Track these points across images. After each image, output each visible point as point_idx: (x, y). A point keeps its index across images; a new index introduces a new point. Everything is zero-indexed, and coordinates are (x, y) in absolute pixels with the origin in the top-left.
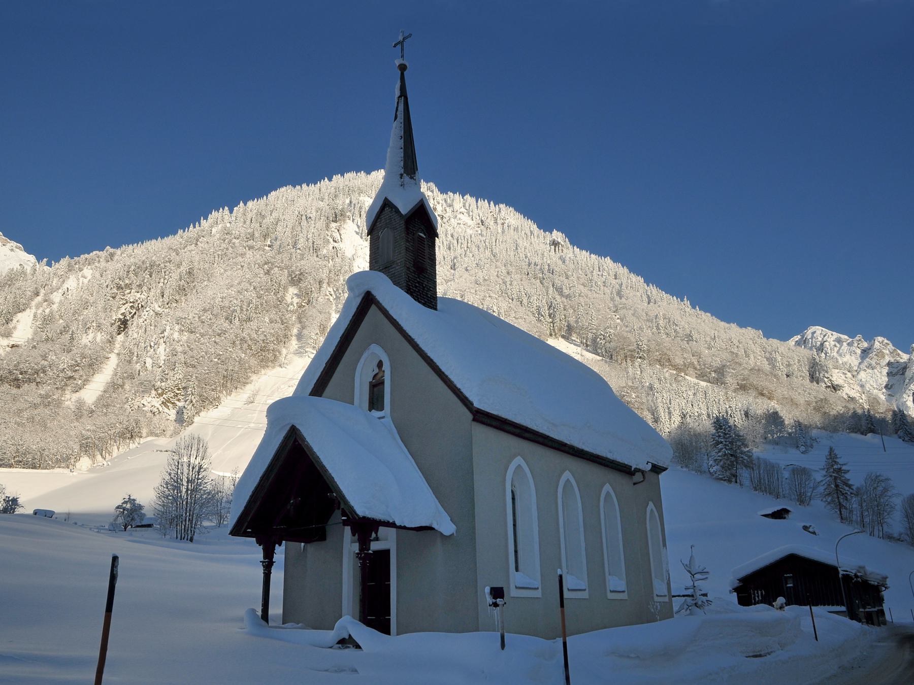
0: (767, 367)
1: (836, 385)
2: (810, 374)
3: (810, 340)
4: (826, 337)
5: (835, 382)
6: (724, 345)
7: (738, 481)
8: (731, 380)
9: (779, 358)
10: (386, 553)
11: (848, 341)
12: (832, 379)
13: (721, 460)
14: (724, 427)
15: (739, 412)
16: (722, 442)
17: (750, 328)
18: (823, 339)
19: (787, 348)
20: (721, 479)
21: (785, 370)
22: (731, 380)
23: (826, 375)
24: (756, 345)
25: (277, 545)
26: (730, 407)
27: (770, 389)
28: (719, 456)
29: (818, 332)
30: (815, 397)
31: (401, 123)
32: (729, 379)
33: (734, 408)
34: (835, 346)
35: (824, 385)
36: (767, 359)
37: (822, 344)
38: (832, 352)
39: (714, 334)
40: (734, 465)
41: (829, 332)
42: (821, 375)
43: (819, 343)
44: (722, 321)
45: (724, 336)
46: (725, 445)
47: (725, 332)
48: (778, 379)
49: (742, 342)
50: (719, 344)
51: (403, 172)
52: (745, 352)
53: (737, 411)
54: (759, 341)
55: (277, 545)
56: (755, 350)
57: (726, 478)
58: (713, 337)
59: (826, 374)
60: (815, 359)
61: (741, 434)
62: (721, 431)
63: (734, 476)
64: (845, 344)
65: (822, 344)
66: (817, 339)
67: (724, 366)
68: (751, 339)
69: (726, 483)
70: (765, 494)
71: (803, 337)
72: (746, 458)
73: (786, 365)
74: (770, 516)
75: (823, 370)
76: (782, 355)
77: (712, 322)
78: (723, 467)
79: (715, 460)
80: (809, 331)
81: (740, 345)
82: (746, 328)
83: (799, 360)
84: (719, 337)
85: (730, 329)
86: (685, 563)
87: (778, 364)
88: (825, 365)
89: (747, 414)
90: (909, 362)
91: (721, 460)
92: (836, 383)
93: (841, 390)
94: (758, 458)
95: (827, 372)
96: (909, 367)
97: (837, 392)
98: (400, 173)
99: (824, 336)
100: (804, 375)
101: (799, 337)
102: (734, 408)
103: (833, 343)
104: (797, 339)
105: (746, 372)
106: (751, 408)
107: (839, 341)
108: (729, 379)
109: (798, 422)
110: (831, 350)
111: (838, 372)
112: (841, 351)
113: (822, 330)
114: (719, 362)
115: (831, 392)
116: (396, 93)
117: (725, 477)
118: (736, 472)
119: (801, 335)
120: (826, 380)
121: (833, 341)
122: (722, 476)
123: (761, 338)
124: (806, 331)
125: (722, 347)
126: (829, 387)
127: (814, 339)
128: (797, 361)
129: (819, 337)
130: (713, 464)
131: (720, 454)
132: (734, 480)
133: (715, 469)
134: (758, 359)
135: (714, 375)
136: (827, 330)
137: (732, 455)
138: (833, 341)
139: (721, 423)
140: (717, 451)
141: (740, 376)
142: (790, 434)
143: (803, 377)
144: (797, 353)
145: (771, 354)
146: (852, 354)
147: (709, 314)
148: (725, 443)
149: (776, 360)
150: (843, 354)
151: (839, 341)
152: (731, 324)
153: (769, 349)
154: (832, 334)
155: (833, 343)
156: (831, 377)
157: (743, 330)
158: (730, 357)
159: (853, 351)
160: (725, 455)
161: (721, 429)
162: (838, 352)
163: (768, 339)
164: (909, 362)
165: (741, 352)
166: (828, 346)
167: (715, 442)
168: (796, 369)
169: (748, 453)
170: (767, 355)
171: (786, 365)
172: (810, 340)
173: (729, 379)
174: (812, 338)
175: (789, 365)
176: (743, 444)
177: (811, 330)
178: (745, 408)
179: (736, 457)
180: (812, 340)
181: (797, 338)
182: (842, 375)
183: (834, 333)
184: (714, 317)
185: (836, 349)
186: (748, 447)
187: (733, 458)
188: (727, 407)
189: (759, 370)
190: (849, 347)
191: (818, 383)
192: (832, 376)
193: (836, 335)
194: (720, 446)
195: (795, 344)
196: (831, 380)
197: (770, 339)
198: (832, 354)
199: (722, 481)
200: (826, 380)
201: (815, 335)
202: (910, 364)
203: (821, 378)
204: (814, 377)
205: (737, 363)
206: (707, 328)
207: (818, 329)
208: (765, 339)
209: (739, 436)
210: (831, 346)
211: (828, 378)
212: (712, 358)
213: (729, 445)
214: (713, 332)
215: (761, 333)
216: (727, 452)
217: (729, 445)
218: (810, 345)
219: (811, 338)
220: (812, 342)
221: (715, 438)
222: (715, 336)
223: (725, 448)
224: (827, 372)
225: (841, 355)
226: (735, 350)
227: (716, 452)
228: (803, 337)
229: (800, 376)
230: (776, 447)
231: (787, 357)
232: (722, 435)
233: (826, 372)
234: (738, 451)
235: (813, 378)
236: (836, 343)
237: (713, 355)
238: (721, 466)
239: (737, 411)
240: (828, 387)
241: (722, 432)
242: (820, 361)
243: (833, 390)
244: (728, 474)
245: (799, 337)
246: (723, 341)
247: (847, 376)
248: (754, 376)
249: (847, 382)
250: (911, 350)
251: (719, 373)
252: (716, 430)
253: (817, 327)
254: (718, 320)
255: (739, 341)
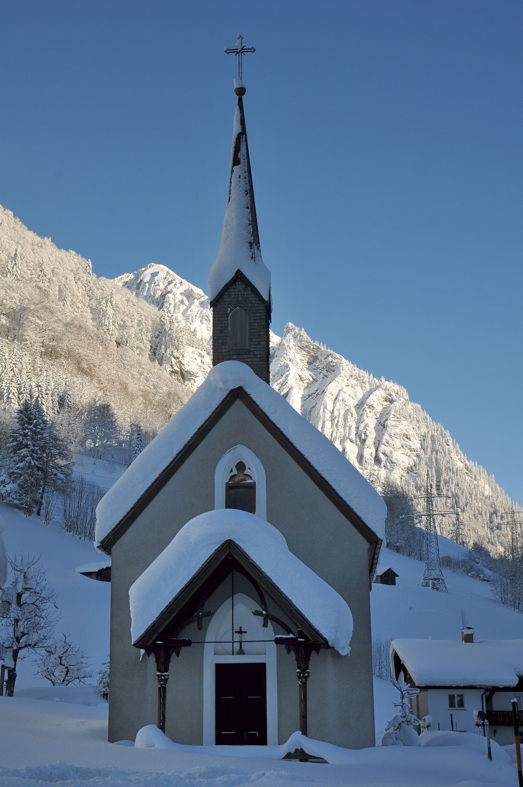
0: (90, 324)
1: (187, 372)
2: (151, 347)
3: (147, 285)
4: (172, 285)
5: (186, 366)
6: (29, 272)
7: (43, 512)
8: (33, 337)
9: (111, 312)
10: (261, 668)
11: (202, 299)
12: (183, 362)
13: (21, 475)
14: (35, 421)
15: (50, 395)
16: (27, 446)
17: (73, 252)
18: (166, 287)
19: (125, 299)
20: (17, 507)
21: (116, 334)
22: (33, 337)
23: (176, 354)
24: (79, 283)
25: (174, 655)
26: (38, 386)
27: (91, 361)
28: (18, 468)
29: (162, 275)
30: (154, 386)
31: (245, 172)
32: (30, 334)
33: (44, 389)
34: (182, 302)
35: (169, 369)
36: (92, 310)
37: (163, 296)
38: (177, 311)
39: (16, 250)
40: (40, 486)
41: (178, 279)
42: (168, 351)
43: (159, 293)
44: (29, 229)
45: (30, 257)
46: (33, 451)
47: (33, 250)
48: (106, 348)
49: (57, 274)
50: (21, 270)
51: (252, 241)
52: (60, 291)
53: (47, 394)
54: (84, 277)
55: (174, 655)
56: (76, 291)
57: (24, 506)
58: (13, 255)
59: (175, 351)
60: (163, 324)
61: (62, 435)
62: (30, 427)
63: (37, 504)
64: (197, 302)
65: (163, 296)
66: (158, 285)
67: (24, 309)
68: (72, 271)
69: (22, 514)
70: (83, 538)
71: (137, 277)
72: (62, 476)
73: (120, 325)
74: (94, 576)
75: (173, 345)
76: (116, 308)
77: (14, 228)
78: (21, 486)
79: (10, 475)
80: (149, 270)
81: (54, 279)
82: (68, 251)
83: (140, 321)
84: (22, 257)
85: (41, 247)
86: (484, 692)
87: (107, 321)
88: (176, 337)
89: (62, 402)
90: (279, 349)
91: (21, 475)
92: (187, 368)
93: (192, 381)
94: (82, 481)
95: (177, 348)
96: (277, 356)
97: (186, 382)
98: (249, 241)
99: (169, 283)
100: (143, 347)
101: (132, 276)
102: (44, 389)
103: (180, 297)
104: (127, 279)
105: (60, 328)
106: (70, 393)
107: (189, 295)
108: (30, 333)
109: (138, 426)
110: (175, 307)
111: (192, 352)
112: (189, 313)
113: (168, 272)
114: (17, 302)
115: (177, 382)
116: (234, 130)
117: (22, 504)
118: (42, 497)
119: (134, 274)
120: (174, 360)
121: (181, 294)
122: (18, 502)
123: (89, 273)
124: (143, 269)
125: (25, 275)
126: (176, 372)
127: (153, 285)
128: (136, 321)
129: (161, 284)
130: (7, 480)
131: (21, 465)
132: (35, 510)
133: (8, 489)
134: (78, 308)
135: (4, 322)
136: (175, 275)
137: (39, 469)
138: (181, 294)
139: (31, 414)
140: (16, 458)
141: (48, 332)
142: (120, 443)
143: (141, 350)
144: (140, 310)
145: (99, 303)
146: (204, 321)
147: (10, 213)
148: (32, 447)
149: (104, 315)
150: (191, 318)
151: (189, 295)
152: (45, 238)
153: (98, 293)
154: (181, 283)
155: (180, 297)
156: (181, 358)
157: (62, 254)
158: (36, 296)
159: (206, 316)
160: (30, 467)
161: (30, 424)
162: (184, 313)
163: (98, 277)
164: (279, 349)
165: (54, 291)
166: (171, 301)
167: (15, 443)
168: (133, 335)
169: (66, 470)
170: (94, 303)
171: (120, 325)
172: (147, 285)
173: (30, 333)
174: (150, 283)
175: (123, 327)
176: (60, 454)
177: (152, 268)
178: (61, 390)
179: (45, 473)
180: (150, 286)
181: (128, 277)
182: (197, 357)
183: (184, 281)
184: (18, 220)
185: (182, 308)
186: (67, 459)
187: (40, 473)
188: (33, 384)
189: (81, 327)
190: (202, 309)
191: (161, 364)
192: (183, 356)
193: (187, 285)
194: (24, 452)
195: (124, 286)
196: (180, 363)
197: (103, 278)
198: (175, 315)
199: (17, 510)
200: (174, 360)
201: (156, 278)
202: (279, 352)
203: (167, 356)
204: (157, 352)
205: (47, 308)
206: (5, 236)
207: (162, 270)
208: (94, 276)
209: (56, 439)
210: (177, 301)
211: (177, 358)
212: (6, 292)
213: (39, 452)
214: (14, 247)
215: (90, 265)
216: (33, 464)
217: (39, 452)
218: (145, 294)
219: (148, 282)
220: (149, 289)
221: (16, 437)
222: (16, 254)
223: (32, 456)
224: (177, 348)
225: (188, 319)
226: (44, 285)
227: (14, 461)
228: (137, 277)
229: (137, 348)
230: (99, 462)
231: (124, 312)
232: (29, 433)
233: (176, 348)
234: (51, 464)
235: (155, 354)
236: (185, 299)
237: (10, 287)
238: (19, 485)
239: (47, 394)
240: (173, 372)
241: (31, 429)
242: (170, 329)
243: (180, 378)
244: (29, 499)
245: (132, 276)
246: (27, 266)
247: (204, 360)
248: (72, 336)
249: (202, 370)
250: (285, 330)
251: (14, 319)
252: (22, 425)
253: (162, 266)
254: (24, 226)
255: (53, 271)
